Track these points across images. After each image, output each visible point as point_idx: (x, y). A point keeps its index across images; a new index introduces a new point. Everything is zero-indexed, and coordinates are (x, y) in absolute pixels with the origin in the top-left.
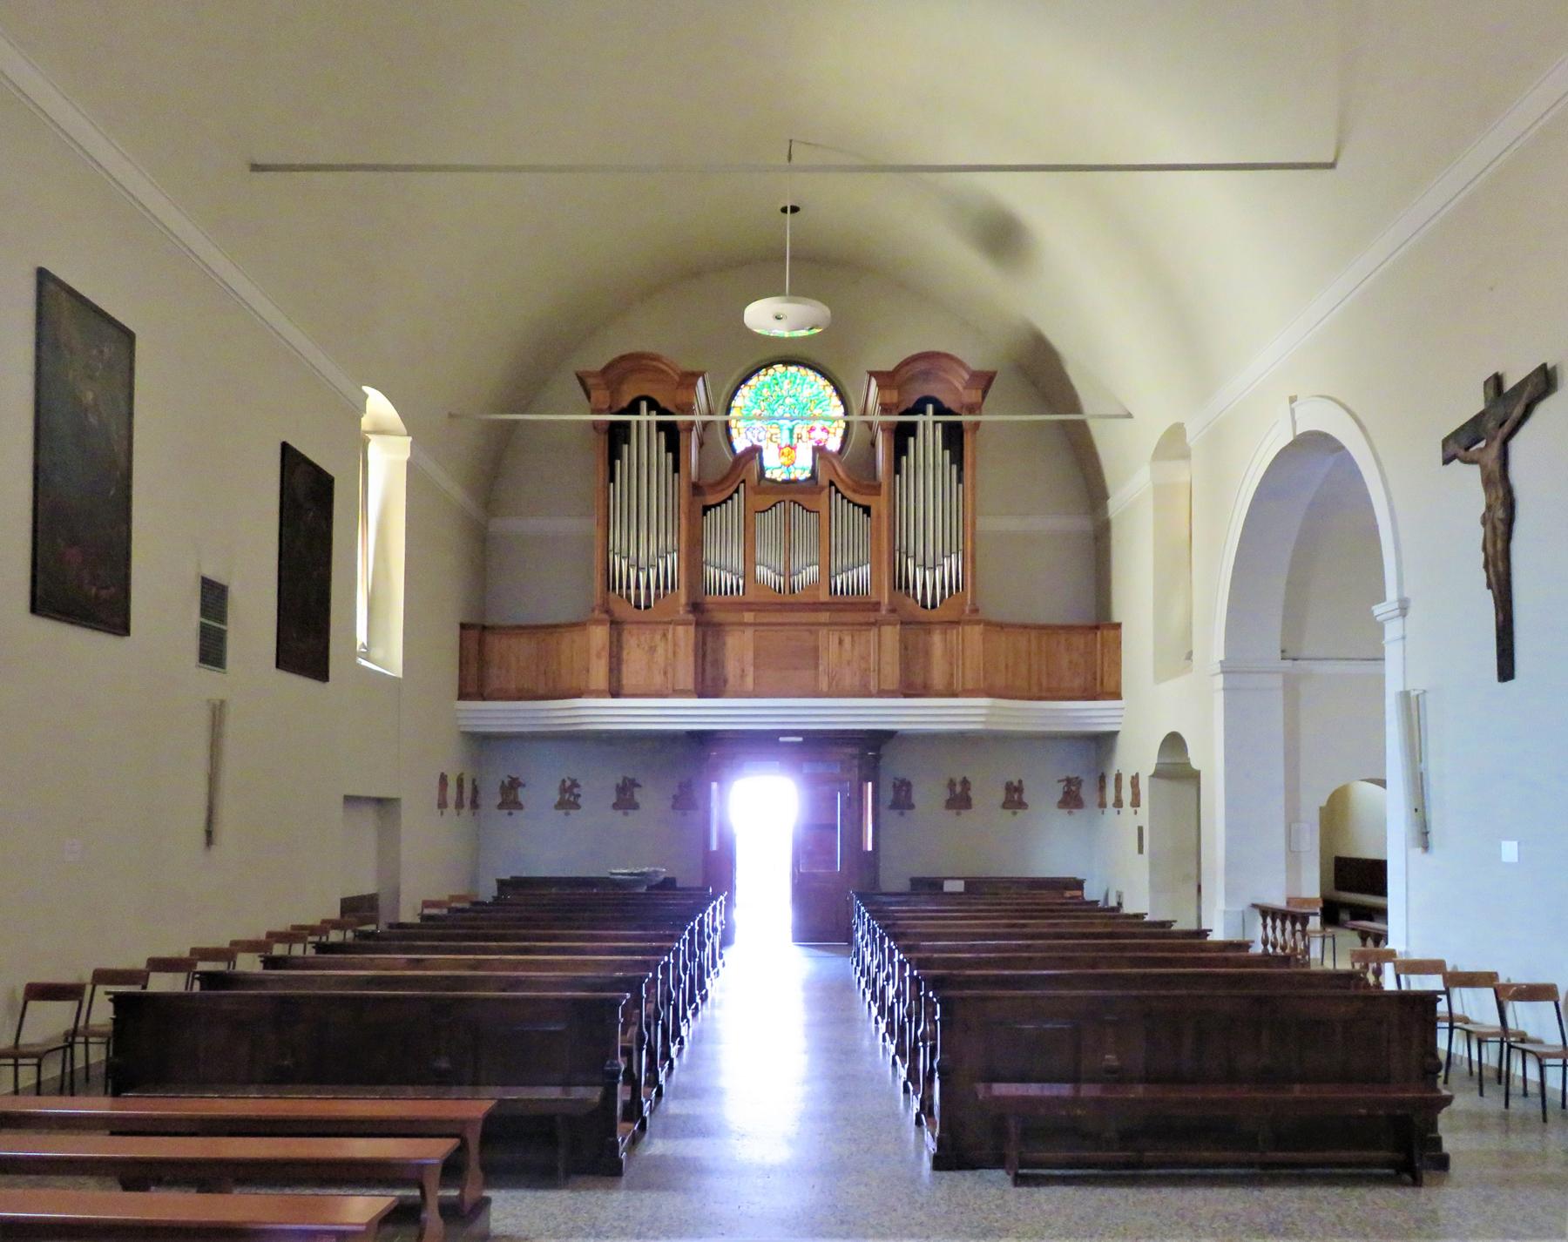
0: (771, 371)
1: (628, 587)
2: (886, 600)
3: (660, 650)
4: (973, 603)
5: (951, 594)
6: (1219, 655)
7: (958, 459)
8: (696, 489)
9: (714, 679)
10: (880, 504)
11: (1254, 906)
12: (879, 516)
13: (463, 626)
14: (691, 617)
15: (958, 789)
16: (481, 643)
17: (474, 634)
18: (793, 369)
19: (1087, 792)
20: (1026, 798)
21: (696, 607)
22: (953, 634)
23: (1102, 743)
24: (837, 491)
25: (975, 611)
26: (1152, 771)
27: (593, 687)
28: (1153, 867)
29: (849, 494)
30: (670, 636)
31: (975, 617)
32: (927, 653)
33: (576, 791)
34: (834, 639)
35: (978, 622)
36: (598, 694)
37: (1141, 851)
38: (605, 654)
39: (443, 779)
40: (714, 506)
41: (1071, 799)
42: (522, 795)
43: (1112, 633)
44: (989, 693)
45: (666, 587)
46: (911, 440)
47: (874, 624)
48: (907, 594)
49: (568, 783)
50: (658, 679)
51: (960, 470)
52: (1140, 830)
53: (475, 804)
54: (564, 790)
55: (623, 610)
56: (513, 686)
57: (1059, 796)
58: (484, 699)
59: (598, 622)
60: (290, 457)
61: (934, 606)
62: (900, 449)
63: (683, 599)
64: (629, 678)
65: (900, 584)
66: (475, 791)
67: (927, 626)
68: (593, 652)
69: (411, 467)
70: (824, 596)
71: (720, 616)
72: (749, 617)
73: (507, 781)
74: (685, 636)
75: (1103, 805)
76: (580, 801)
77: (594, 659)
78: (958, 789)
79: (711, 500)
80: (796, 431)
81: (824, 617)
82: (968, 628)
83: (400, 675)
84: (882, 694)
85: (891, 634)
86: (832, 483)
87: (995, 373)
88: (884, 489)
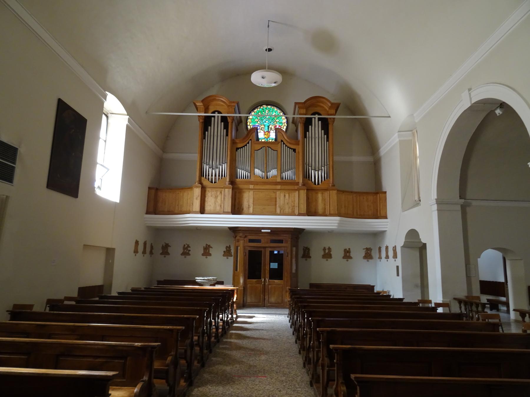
0: (262, 107)
1: (209, 176)
2: (301, 181)
3: (219, 198)
4: (333, 183)
5: (324, 179)
6: (434, 195)
7: (327, 133)
8: (233, 142)
9: (238, 208)
10: (299, 148)
11: (455, 299)
12: (299, 152)
13: (149, 188)
14: (231, 186)
15: (327, 251)
16: (156, 196)
17: (153, 192)
18: (269, 107)
19: (375, 254)
20: (352, 255)
21: (232, 182)
22: (326, 194)
23: (378, 235)
24: (284, 144)
25: (334, 186)
26: (402, 244)
27: (194, 210)
28: (404, 281)
29: (288, 145)
30: (223, 192)
31: (333, 188)
32: (316, 201)
33: (189, 249)
34: (282, 195)
35: (334, 190)
36: (196, 213)
37: (398, 275)
38: (199, 198)
39: (137, 243)
40: (240, 148)
41: (368, 255)
42: (170, 250)
43: (383, 195)
44: (339, 215)
45: (222, 176)
46: (310, 126)
47: (296, 190)
48: (309, 180)
49: (186, 246)
50: (218, 208)
51: (328, 138)
52: (398, 267)
53: (151, 253)
54: (184, 248)
55: (206, 182)
56: (166, 210)
57: (363, 254)
58: (155, 214)
59: (197, 187)
60: (62, 107)
61: (318, 184)
62: (306, 130)
63: (228, 180)
64: (207, 208)
65: (307, 176)
66: (152, 247)
67: (316, 191)
68: (195, 198)
69: (129, 129)
70: (279, 180)
71: (241, 186)
72: (251, 187)
73: (164, 244)
74: (228, 192)
75: (380, 258)
76: (190, 253)
77: (195, 200)
78: (327, 251)
79: (239, 145)
80: (270, 127)
81: (279, 187)
82: (331, 192)
83: (118, 201)
84: (300, 215)
85: (303, 193)
86: (282, 141)
87: (340, 104)
88: (301, 143)
